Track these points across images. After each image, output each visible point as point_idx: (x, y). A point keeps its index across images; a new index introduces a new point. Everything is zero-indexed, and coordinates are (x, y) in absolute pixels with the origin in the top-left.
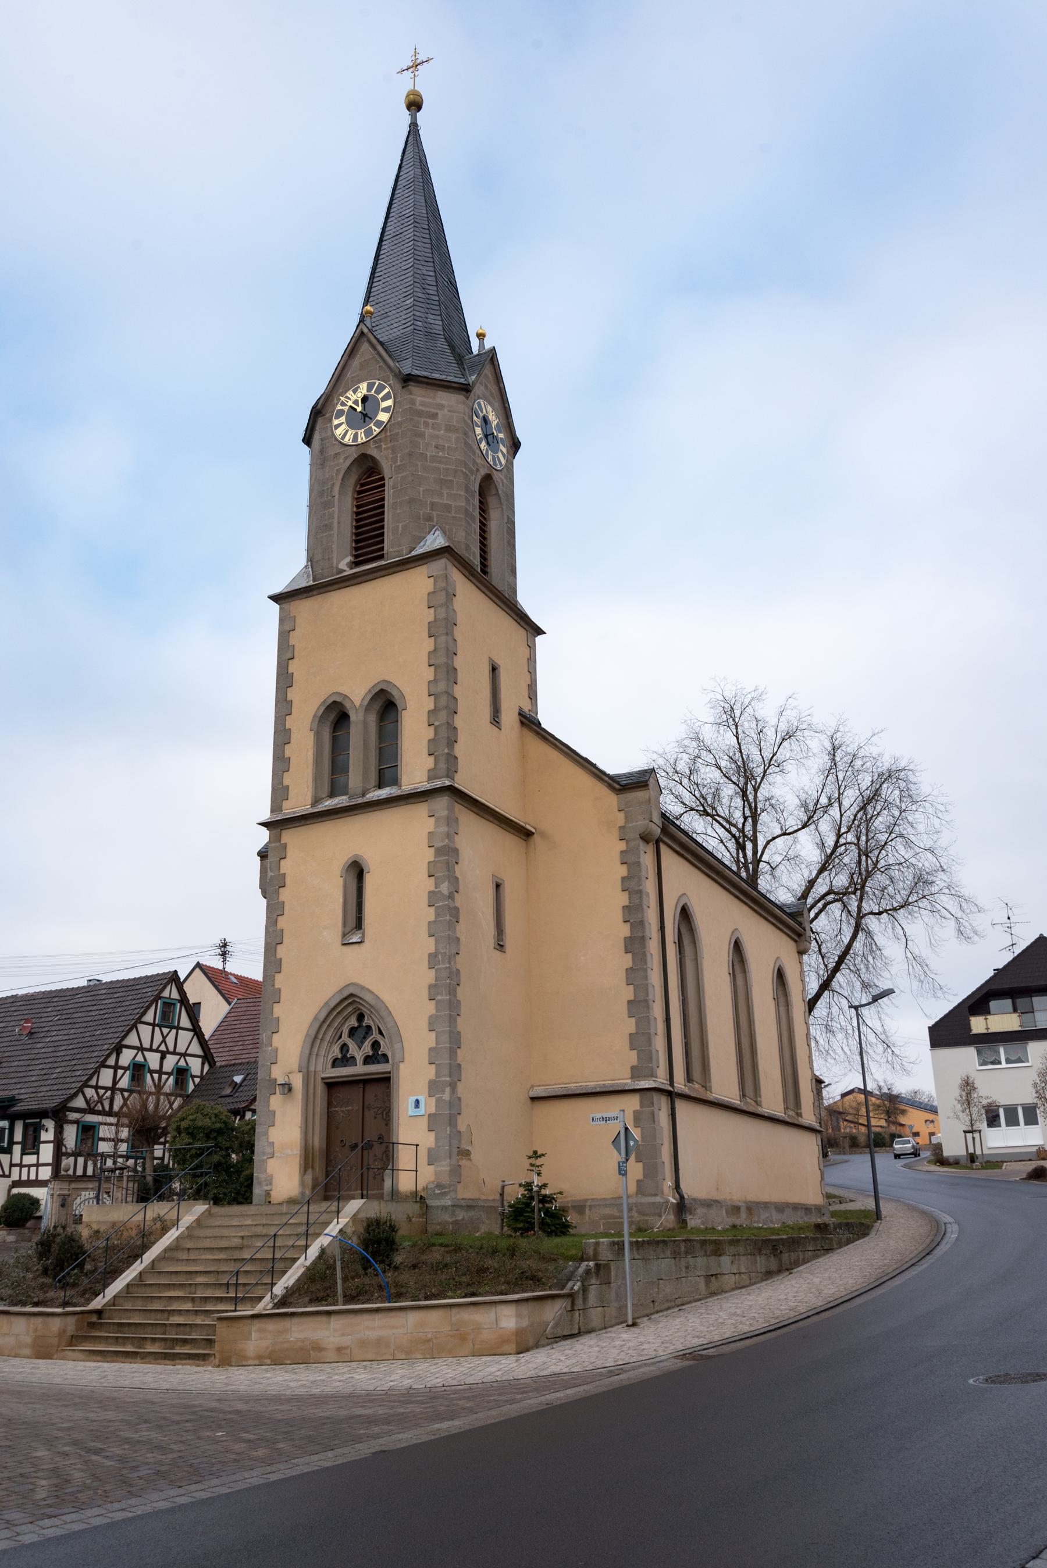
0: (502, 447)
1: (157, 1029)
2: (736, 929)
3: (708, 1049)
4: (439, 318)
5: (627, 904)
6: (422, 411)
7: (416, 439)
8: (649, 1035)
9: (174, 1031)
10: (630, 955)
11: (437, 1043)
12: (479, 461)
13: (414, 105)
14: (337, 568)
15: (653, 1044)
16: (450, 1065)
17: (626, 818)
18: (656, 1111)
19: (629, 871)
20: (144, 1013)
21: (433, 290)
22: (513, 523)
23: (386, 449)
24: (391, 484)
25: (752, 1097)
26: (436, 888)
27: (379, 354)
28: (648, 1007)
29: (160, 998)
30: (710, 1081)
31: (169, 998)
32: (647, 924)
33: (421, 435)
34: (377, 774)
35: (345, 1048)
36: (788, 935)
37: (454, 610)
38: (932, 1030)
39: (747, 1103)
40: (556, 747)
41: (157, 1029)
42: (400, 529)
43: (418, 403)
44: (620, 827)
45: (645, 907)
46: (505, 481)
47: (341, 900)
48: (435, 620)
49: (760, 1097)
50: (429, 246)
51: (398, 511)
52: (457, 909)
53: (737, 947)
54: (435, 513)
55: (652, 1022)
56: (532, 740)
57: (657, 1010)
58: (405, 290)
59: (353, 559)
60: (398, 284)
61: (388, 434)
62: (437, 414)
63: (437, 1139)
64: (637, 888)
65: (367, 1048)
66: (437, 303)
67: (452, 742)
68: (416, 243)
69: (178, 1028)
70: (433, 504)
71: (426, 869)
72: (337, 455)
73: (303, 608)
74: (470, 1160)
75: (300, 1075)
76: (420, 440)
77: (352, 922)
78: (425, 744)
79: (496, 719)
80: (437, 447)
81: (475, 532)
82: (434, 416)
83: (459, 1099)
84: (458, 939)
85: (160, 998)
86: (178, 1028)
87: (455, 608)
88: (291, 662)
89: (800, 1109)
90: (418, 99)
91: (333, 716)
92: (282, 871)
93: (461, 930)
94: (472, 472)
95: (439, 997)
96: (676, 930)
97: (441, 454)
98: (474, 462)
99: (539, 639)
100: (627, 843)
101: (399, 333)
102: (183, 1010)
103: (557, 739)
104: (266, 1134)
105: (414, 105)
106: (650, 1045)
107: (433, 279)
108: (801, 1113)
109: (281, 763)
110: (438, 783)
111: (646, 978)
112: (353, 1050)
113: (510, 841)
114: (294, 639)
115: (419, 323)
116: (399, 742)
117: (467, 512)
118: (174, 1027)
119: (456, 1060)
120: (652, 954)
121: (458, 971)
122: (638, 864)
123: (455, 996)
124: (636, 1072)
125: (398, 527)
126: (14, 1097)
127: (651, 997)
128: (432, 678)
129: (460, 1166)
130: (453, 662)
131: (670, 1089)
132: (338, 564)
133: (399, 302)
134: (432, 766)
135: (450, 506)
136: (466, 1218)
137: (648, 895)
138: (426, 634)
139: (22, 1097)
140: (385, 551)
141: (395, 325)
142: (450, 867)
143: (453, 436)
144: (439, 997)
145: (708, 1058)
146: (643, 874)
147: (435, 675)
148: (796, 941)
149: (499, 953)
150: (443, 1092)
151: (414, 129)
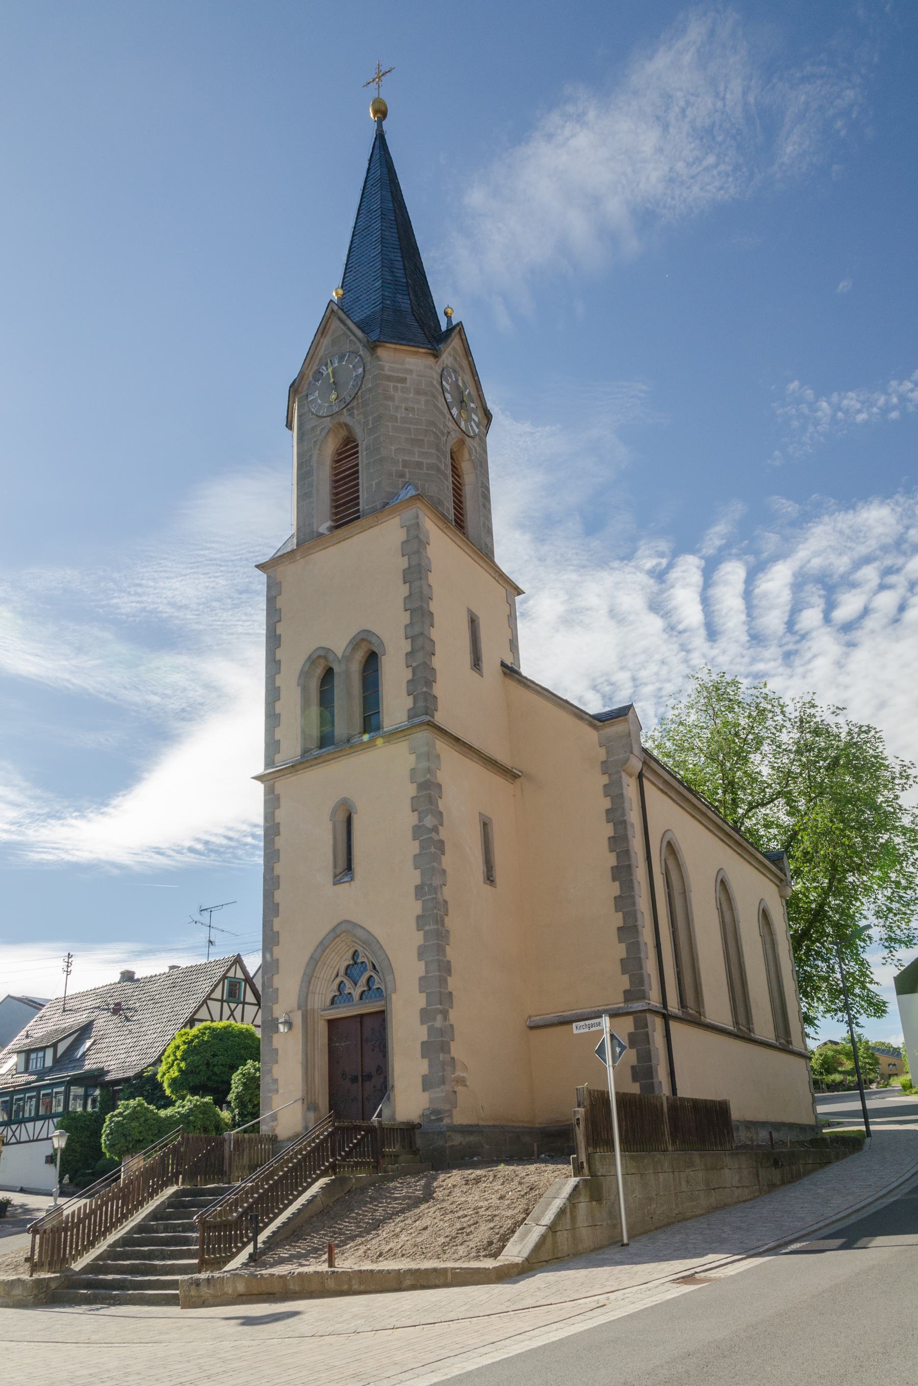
0: (474, 417)
1: (225, 1004)
2: (721, 869)
3: (699, 976)
4: (407, 297)
5: (612, 834)
6: (391, 376)
7: (386, 402)
8: (640, 958)
9: (240, 1006)
10: (617, 883)
11: (427, 972)
12: (451, 425)
13: (382, 113)
14: (317, 532)
15: (644, 968)
16: (440, 993)
17: (607, 753)
18: (650, 1033)
19: (612, 803)
20: (213, 991)
21: (400, 273)
22: (488, 489)
23: (358, 415)
24: (364, 446)
25: (744, 1024)
26: (419, 822)
27: (349, 329)
28: (637, 931)
29: (227, 978)
30: (703, 1007)
31: (235, 978)
32: (633, 854)
33: (391, 398)
34: (362, 721)
35: (342, 985)
36: (771, 880)
37: (427, 557)
38: (897, 979)
39: (739, 1029)
40: (538, 693)
41: (225, 1004)
42: (374, 486)
43: (386, 369)
44: (603, 763)
45: (630, 836)
46: (478, 448)
47: (331, 842)
48: (409, 567)
49: (753, 1024)
50: (396, 235)
51: (372, 471)
52: (442, 842)
53: (723, 884)
54: (407, 470)
55: (642, 947)
56: (512, 685)
57: (647, 935)
58: (373, 275)
59: (333, 524)
60: (368, 270)
61: (360, 401)
62: (406, 379)
63: (430, 1066)
64: (621, 819)
65: (361, 986)
66: (405, 284)
67: (430, 682)
68: (383, 232)
69: (244, 1003)
70: (404, 461)
71: (410, 806)
72: (313, 429)
73: (288, 572)
74: (466, 1086)
75: (299, 1013)
76: (390, 403)
77: (342, 864)
78: (404, 685)
79: (476, 663)
80: (406, 409)
81: (448, 488)
82: (404, 380)
83: (452, 1026)
84: (444, 871)
85: (227, 978)
86: (244, 1003)
87: (429, 556)
88: (278, 624)
89: (790, 1037)
90: (383, 108)
91: (319, 672)
92: (277, 821)
93: (447, 861)
94: (443, 434)
95: (427, 928)
96: (663, 863)
97: (411, 415)
98: (445, 425)
99: (518, 599)
100: (610, 775)
101: (369, 313)
102: (248, 985)
103: (537, 685)
104: (270, 1071)
105: (382, 113)
106: (641, 968)
107: (401, 263)
108: (791, 1041)
109: (273, 718)
110: (417, 720)
111: (634, 904)
112: (349, 987)
113: (498, 781)
114: (280, 602)
115: (388, 302)
116: (380, 689)
117: (438, 469)
118: (241, 1003)
119: (447, 988)
120: (639, 882)
121: (446, 902)
122: (621, 796)
123: (443, 925)
124: (629, 996)
125: (372, 485)
126: (103, 1068)
127: (639, 923)
128: (408, 621)
129: (455, 1092)
130: (428, 606)
131: (664, 1011)
132: (318, 527)
133: (369, 286)
134: (411, 705)
135: (422, 463)
136: (464, 1143)
137: (633, 825)
138: (402, 581)
139: (111, 1068)
140: (361, 507)
141: (365, 307)
142: (431, 800)
143: (423, 399)
144: (427, 928)
145: (701, 985)
146: (627, 805)
147: (411, 619)
148: (778, 886)
149: (488, 887)
150: (435, 1019)
151: (380, 140)
